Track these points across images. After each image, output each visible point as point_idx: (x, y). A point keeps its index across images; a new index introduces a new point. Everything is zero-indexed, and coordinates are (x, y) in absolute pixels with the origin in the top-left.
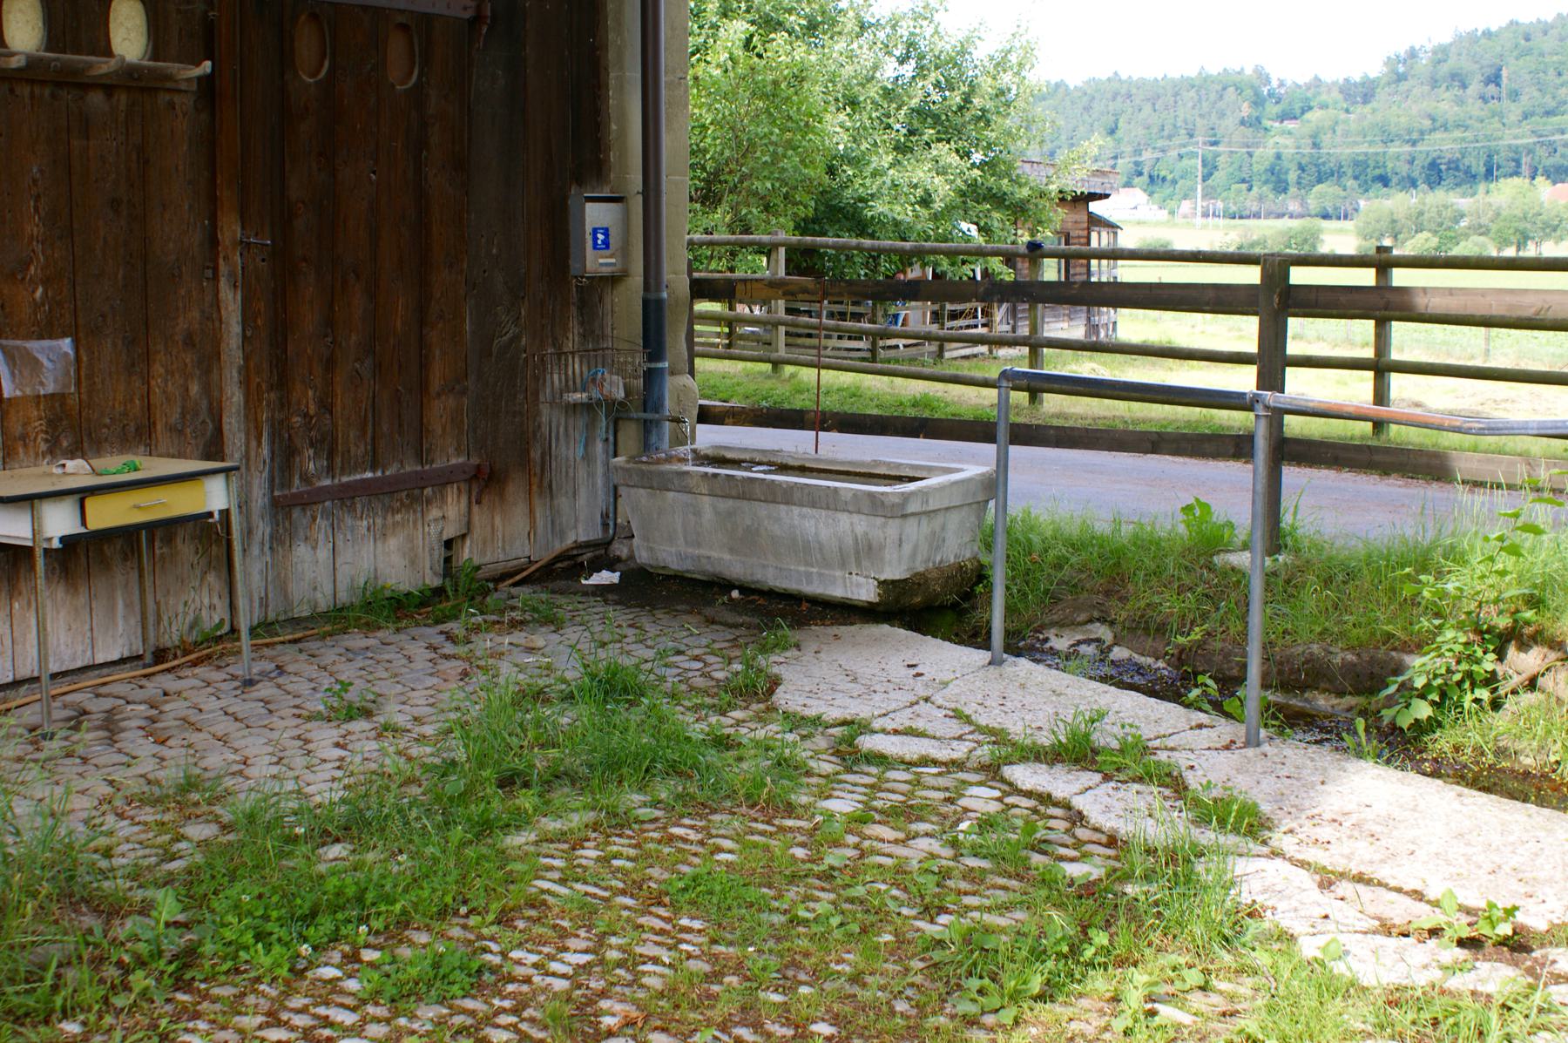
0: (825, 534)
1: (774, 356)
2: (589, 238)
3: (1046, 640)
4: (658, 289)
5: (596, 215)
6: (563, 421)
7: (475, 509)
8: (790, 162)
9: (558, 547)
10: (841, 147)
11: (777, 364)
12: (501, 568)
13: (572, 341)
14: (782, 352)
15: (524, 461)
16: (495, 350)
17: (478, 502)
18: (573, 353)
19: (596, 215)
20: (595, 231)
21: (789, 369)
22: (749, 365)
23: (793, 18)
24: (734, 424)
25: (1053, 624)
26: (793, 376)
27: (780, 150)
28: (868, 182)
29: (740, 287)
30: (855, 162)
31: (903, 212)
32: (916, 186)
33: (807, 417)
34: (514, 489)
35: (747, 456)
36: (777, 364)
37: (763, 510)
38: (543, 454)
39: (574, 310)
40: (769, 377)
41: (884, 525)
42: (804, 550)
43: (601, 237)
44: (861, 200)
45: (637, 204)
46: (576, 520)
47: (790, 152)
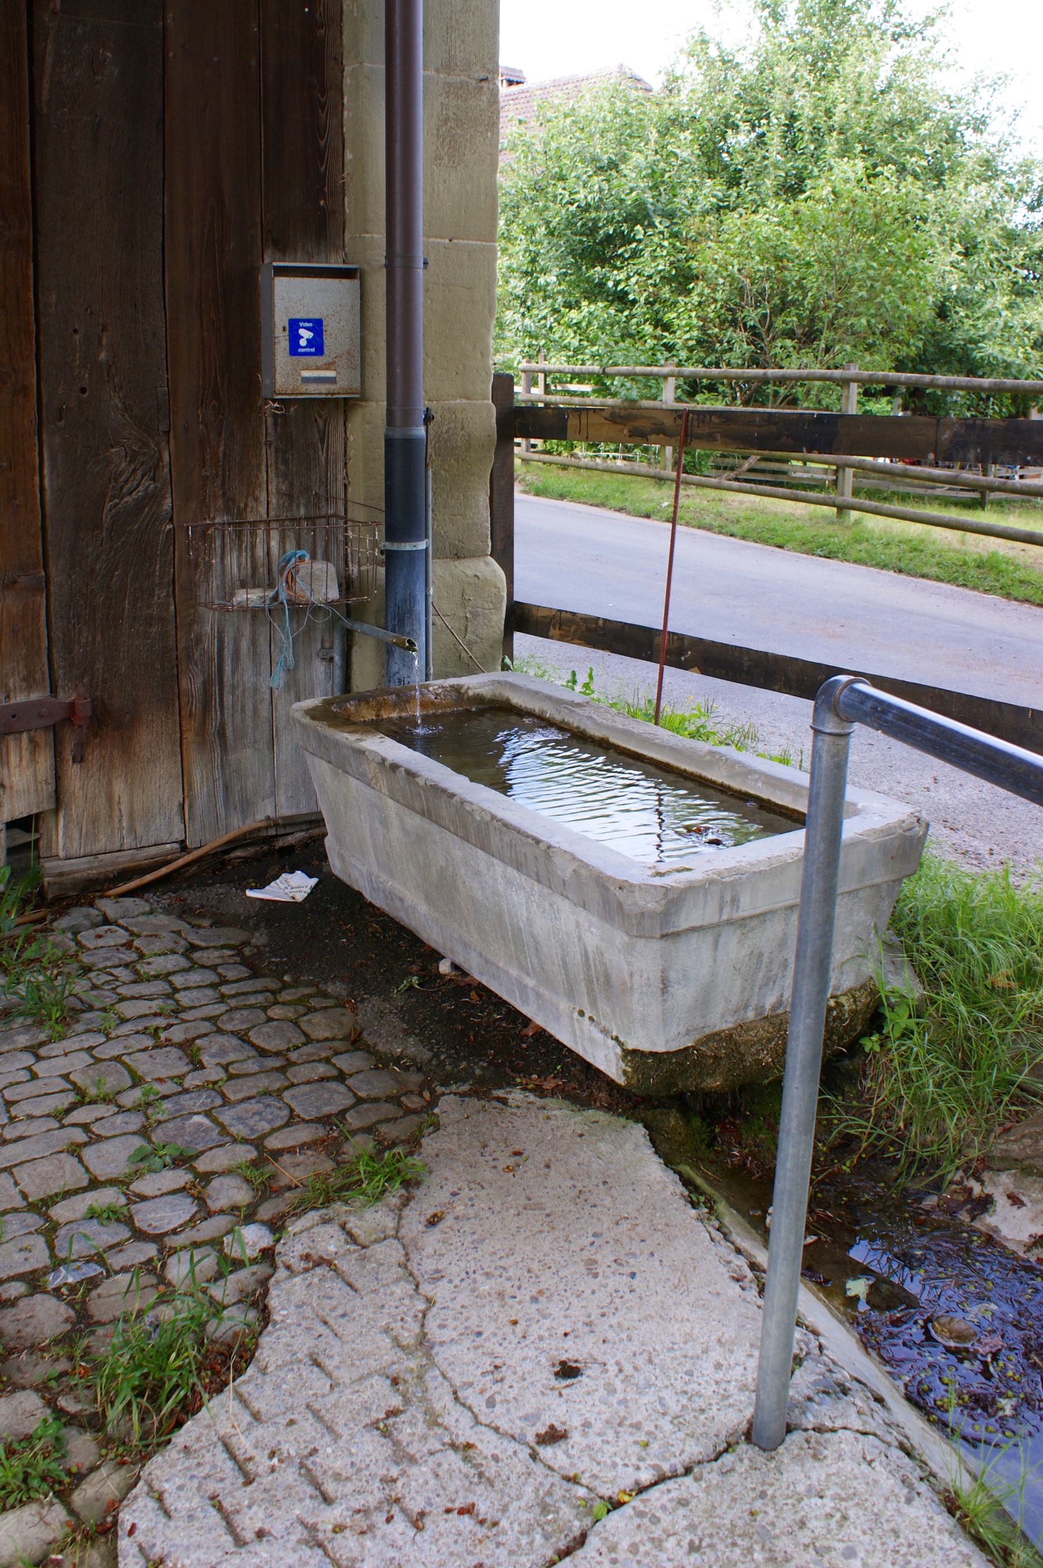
0: (541, 926)
1: (839, 500)
2: (282, 343)
3: (985, 1203)
4: (408, 420)
5: (292, 297)
6: (247, 631)
7: (73, 773)
8: (889, 297)
9: (238, 825)
10: (954, 288)
11: (842, 509)
12: (124, 859)
13: (266, 499)
14: (849, 498)
15: (169, 692)
16: (107, 517)
17: (79, 759)
18: (268, 523)
19: (292, 297)
20: (294, 325)
21: (854, 514)
22: (813, 506)
23: (913, 160)
24: (562, 638)
25: (1008, 1163)
26: (857, 522)
27: (878, 285)
28: (980, 324)
29: (572, 421)
30: (968, 304)
31: (1013, 354)
32: (1029, 329)
33: (658, 640)
34: (152, 738)
35: (535, 706)
36: (842, 509)
37: (459, 850)
38: (207, 684)
39: (267, 455)
40: (832, 523)
41: (629, 949)
42: (516, 939)
43: (306, 334)
44: (972, 341)
45: (378, 283)
46: (274, 785)
47: (888, 288)
